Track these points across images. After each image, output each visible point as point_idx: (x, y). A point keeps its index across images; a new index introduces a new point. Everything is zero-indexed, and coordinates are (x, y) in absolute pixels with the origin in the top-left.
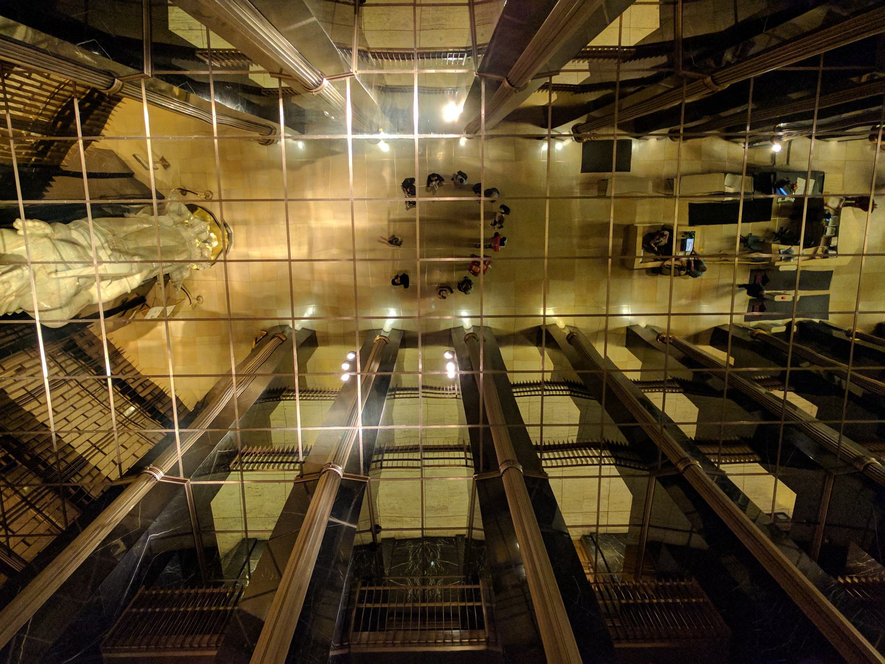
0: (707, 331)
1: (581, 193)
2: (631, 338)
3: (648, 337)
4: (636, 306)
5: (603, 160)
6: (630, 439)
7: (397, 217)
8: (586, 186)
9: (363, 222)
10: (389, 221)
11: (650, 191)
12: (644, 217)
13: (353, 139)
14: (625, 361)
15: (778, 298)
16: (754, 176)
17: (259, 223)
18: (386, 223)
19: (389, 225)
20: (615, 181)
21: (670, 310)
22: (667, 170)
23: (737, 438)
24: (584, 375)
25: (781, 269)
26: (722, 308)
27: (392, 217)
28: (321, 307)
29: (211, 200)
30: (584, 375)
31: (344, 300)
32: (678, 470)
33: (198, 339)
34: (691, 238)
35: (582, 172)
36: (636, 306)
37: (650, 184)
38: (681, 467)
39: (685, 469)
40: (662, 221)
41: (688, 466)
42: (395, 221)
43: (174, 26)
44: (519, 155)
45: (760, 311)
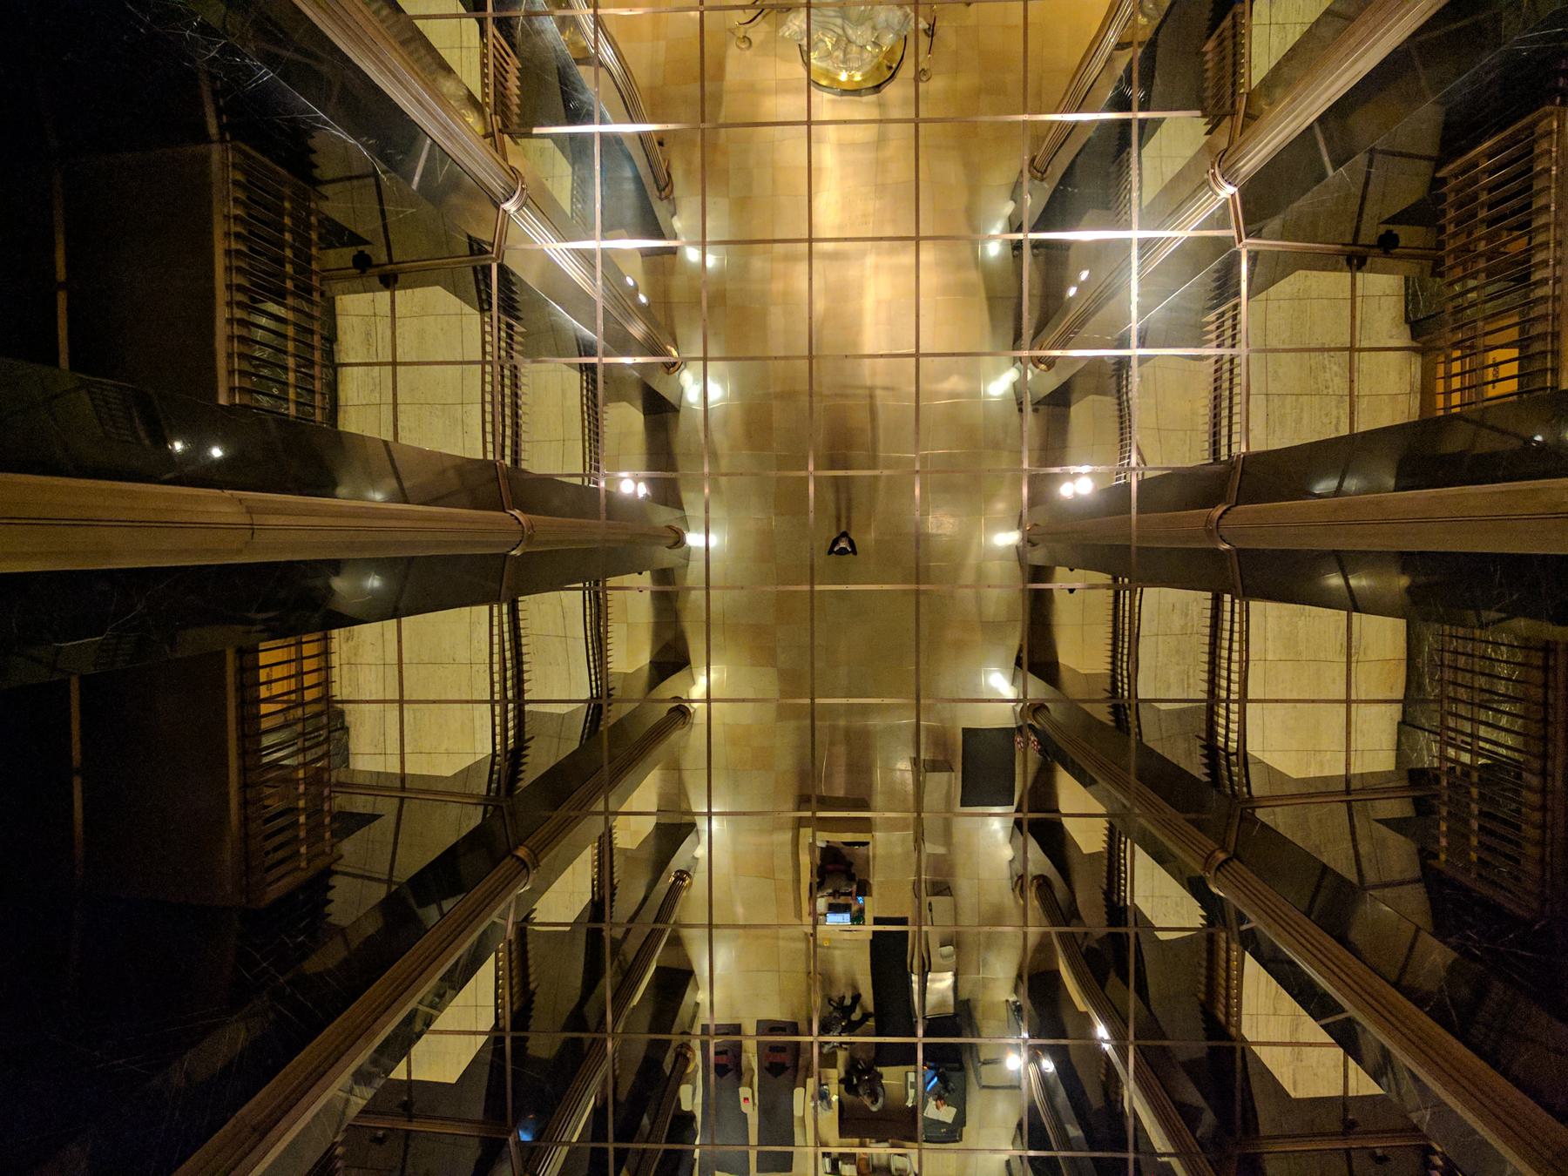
0: (689, 963)
1: (928, 728)
2: (674, 831)
3: (678, 862)
4: (727, 847)
5: (982, 767)
6: (536, 795)
7: (879, 402)
8: (940, 739)
9: (873, 339)
10: (872, 389)
11: (931, 848)
12: (887, 846)
13: (1130, 240)
14: (634, 817)
15: (744, 1092)
16: (955, 1015)
17: (880, 165)
18: (868, 383)
19: (866, 388)
20: (945, 785)
21: (718, 926)
22: (963, 885)
23: (532, 986)
24: (619, 739)
25: (798, 1092)
26: (731, 985)
27: (879, 393)
28: (721, 274)
29: (917, 80)
30: (619, 739)
31: (731, 314)
32: (516, 848)
33: (662, 43)
34: (853, 920)
35: (964, 729)
36: (727, 847)
37: (941, 850)
38: (522, 852)
39: (519, 858)
40: (876, 880)
41: (526, 866)
42: (872, 397)
43: (449, 1072)
44: (991, 629)
45: (717, 1066)
